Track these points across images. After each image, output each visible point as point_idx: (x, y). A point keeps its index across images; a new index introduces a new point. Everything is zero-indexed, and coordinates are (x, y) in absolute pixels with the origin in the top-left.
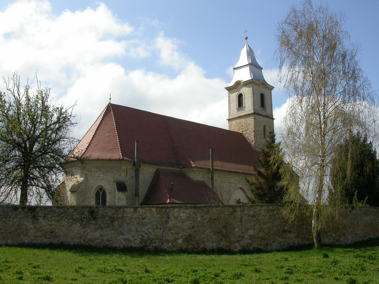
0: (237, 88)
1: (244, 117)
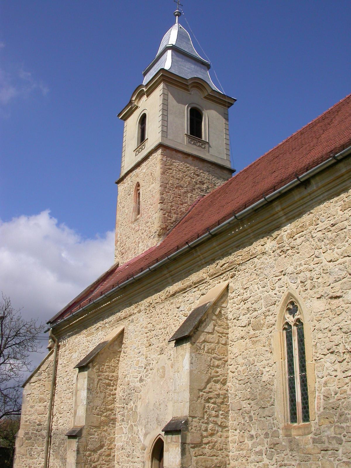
0: (188, 90)
1: (210, 165)
